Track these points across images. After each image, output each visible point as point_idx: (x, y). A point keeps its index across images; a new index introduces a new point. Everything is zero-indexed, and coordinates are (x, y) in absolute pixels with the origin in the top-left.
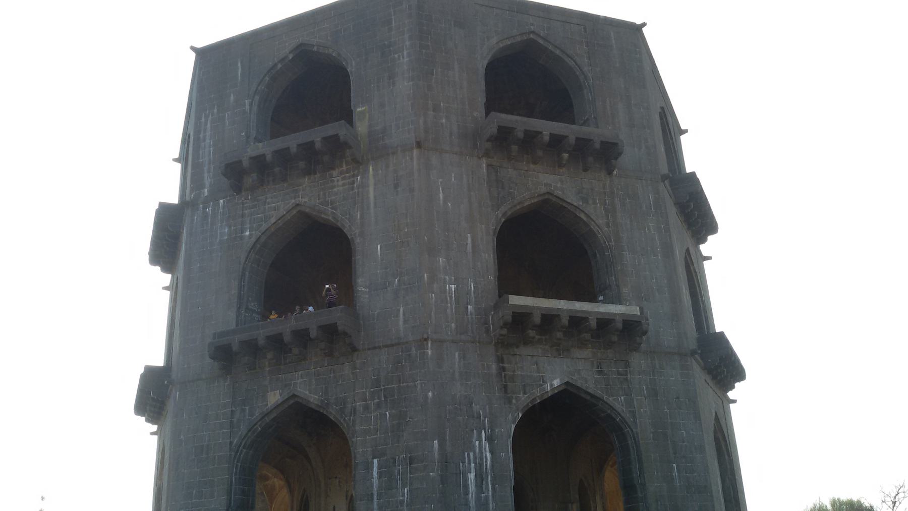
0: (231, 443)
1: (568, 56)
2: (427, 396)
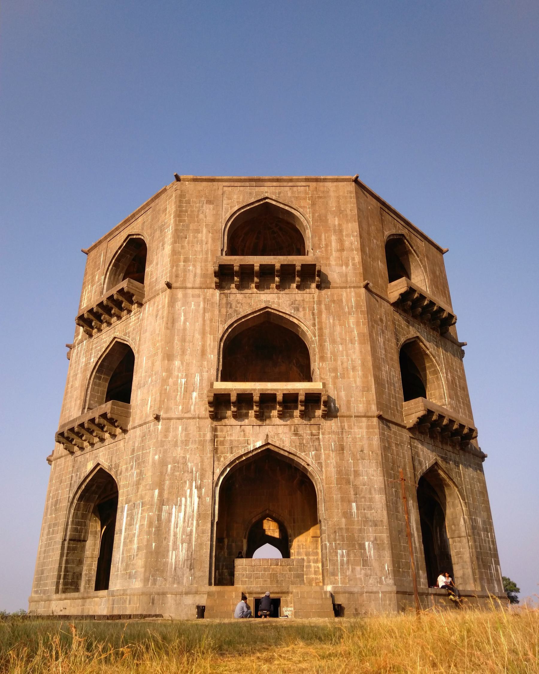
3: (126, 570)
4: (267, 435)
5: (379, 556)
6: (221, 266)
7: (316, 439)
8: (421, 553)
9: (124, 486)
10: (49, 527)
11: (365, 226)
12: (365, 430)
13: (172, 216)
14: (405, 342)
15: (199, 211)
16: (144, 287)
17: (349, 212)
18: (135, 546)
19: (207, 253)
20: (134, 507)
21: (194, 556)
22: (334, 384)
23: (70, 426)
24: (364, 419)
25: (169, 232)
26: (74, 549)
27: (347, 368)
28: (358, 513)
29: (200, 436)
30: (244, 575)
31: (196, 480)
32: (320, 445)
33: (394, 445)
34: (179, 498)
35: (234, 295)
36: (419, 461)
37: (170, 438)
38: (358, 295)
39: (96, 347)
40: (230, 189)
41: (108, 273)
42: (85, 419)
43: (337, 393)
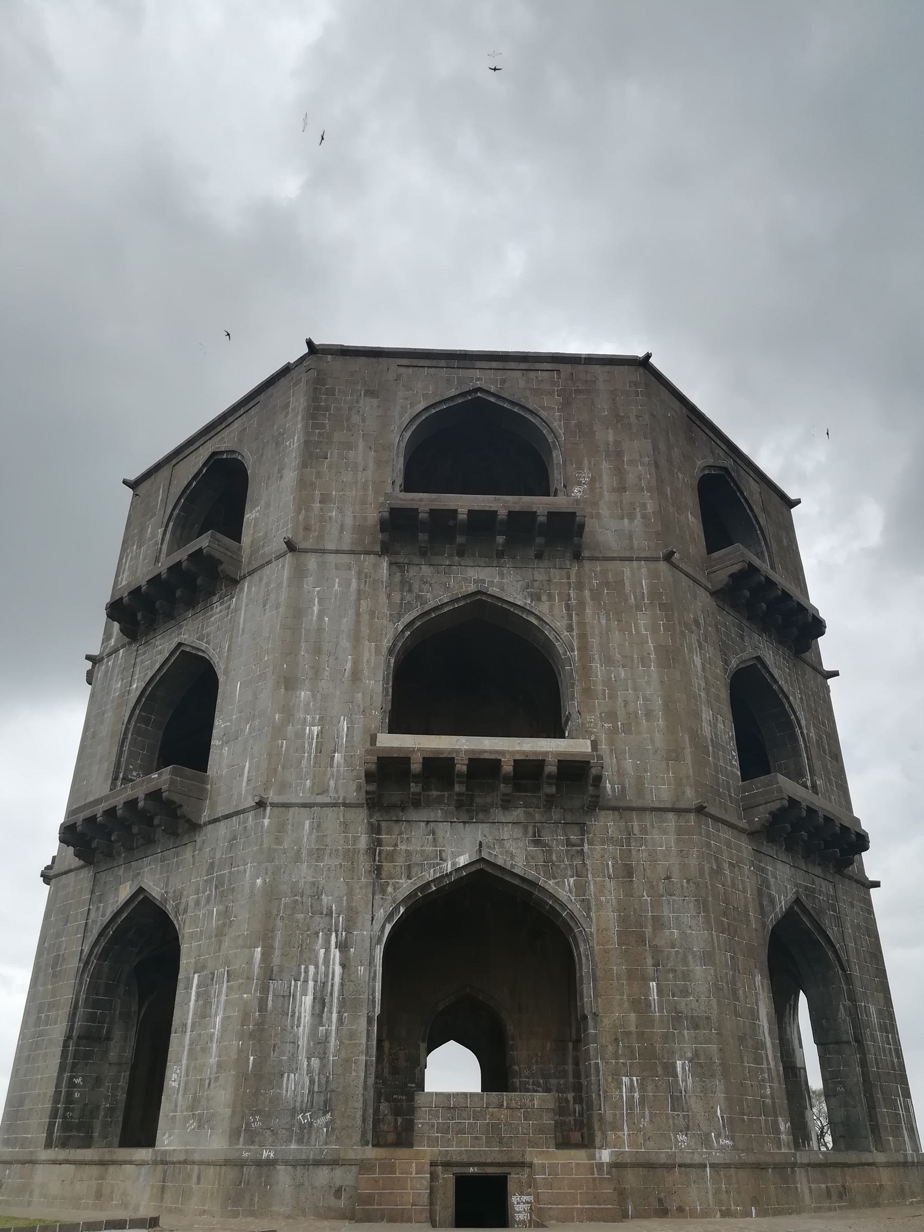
0: (82, 951)
1: (531, 412)
2: (254, 883)
3: (192, 1108)
4: (481, 844)
5: (704, 1090)
6: (393, 511)
7: (578, 852)
8: (779, 1081)
9: (192, 936)
10: (40, 1011)
11: (662, 446)
12: (672, 838)
13: (300, 417)
14: (737, 666)
15: (350, 409)
16: (240, 548)
17: (633, 420)
18: (213, 1060)
19: (365, 489)
20: (212, 980)
21: (333, 1086)
22: (611, 743)
23: (87, 813)
24: (671, 816)
25: (294, 444)
26: (88, 1055)
27: (636, 713)
28: (660, 1002)
29: (346, 842)
30: (433, 1126)
31: (336, 931)
32: (584, 864)
33: (726, 866)
34: (303, 967)
35: (417, 568)
36: (770, 895)
37: (286, 845)
38: (653, 575)
39: (142, 662)
40: (410, 370)
41: (171, 524)
42: (119, 801)
43: (617, 762)
